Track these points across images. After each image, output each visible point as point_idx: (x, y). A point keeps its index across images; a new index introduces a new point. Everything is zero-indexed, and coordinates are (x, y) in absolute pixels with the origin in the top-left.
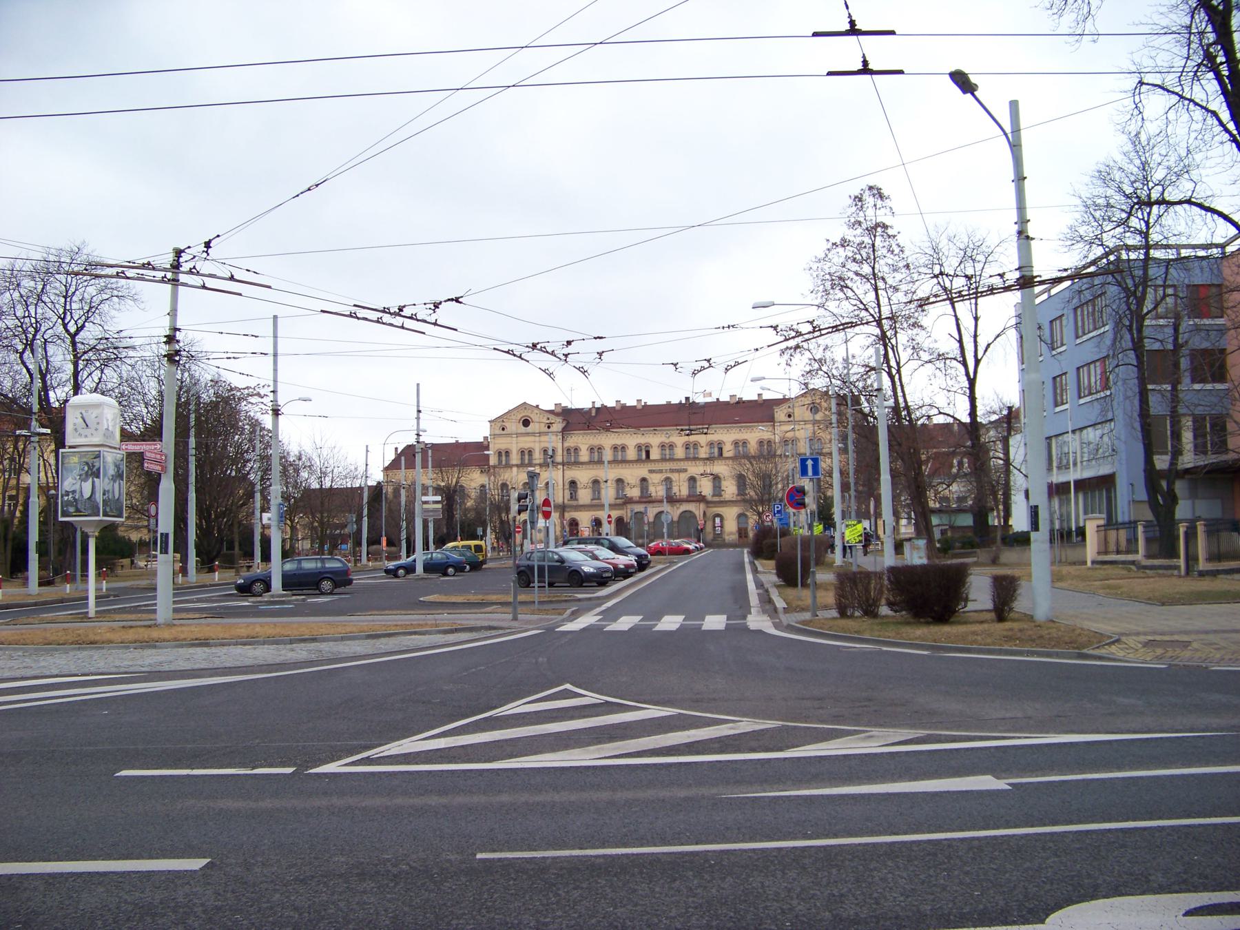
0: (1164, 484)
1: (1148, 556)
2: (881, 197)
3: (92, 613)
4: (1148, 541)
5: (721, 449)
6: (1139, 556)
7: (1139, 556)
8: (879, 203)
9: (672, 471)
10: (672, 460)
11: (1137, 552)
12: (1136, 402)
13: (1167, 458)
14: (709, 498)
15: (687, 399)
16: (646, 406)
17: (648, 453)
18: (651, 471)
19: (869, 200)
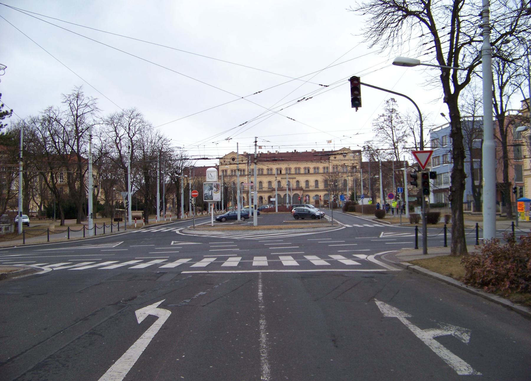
0: (477, 190)
1: (474, 211)
2: (394, 101)
3: (213, 224)
4: (474, 206)
5: (309, 170)
6: (472, 211)
7: (472, 211)
8: (394, 103)
9: (290, 178)
10: (290, 174)
11: (470, 210)
12: (470, 166)
13: (479, 181)
14: (304, 189)
15: (295, 151)
16: (279, 153)
17: (281, 171)
18: (282, 178)
19: (391, 102)
